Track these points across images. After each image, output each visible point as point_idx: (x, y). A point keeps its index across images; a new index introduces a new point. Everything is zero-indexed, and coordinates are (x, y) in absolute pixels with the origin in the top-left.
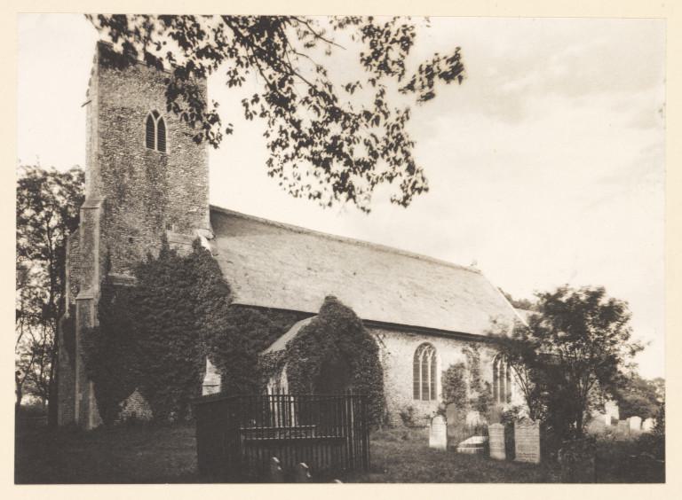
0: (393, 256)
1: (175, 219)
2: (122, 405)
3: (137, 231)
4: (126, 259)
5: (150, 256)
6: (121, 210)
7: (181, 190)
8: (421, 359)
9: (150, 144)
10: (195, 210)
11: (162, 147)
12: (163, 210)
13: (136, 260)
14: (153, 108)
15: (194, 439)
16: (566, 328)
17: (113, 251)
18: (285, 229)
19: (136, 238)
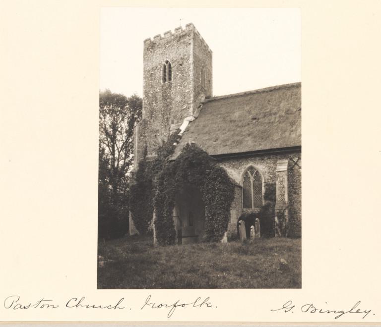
0: (270, 92)
1: (175, 117)
2: (149, 223)
3: (158, 130)
4: (154, 147)
5: (164, 142)
6: (152, 121)
7: (178, 98)
8: (249, 154)
9: (164, 81)
10: (185, 107)
11: (170, 79)
12: (170, 114)
13: (158, 145)
14: (165, 60)
15: (235, 197)
16: (105, 104)
17: (148, 144)
18: (229, 98)
19: (158, 134)
